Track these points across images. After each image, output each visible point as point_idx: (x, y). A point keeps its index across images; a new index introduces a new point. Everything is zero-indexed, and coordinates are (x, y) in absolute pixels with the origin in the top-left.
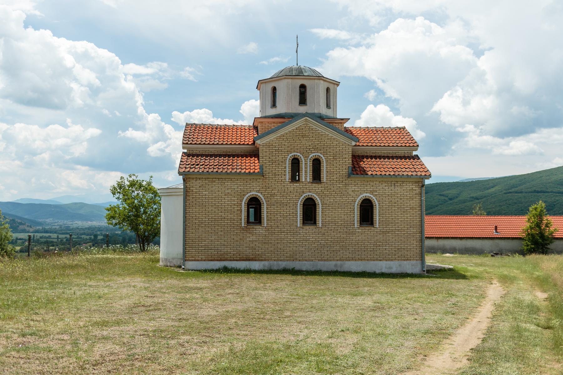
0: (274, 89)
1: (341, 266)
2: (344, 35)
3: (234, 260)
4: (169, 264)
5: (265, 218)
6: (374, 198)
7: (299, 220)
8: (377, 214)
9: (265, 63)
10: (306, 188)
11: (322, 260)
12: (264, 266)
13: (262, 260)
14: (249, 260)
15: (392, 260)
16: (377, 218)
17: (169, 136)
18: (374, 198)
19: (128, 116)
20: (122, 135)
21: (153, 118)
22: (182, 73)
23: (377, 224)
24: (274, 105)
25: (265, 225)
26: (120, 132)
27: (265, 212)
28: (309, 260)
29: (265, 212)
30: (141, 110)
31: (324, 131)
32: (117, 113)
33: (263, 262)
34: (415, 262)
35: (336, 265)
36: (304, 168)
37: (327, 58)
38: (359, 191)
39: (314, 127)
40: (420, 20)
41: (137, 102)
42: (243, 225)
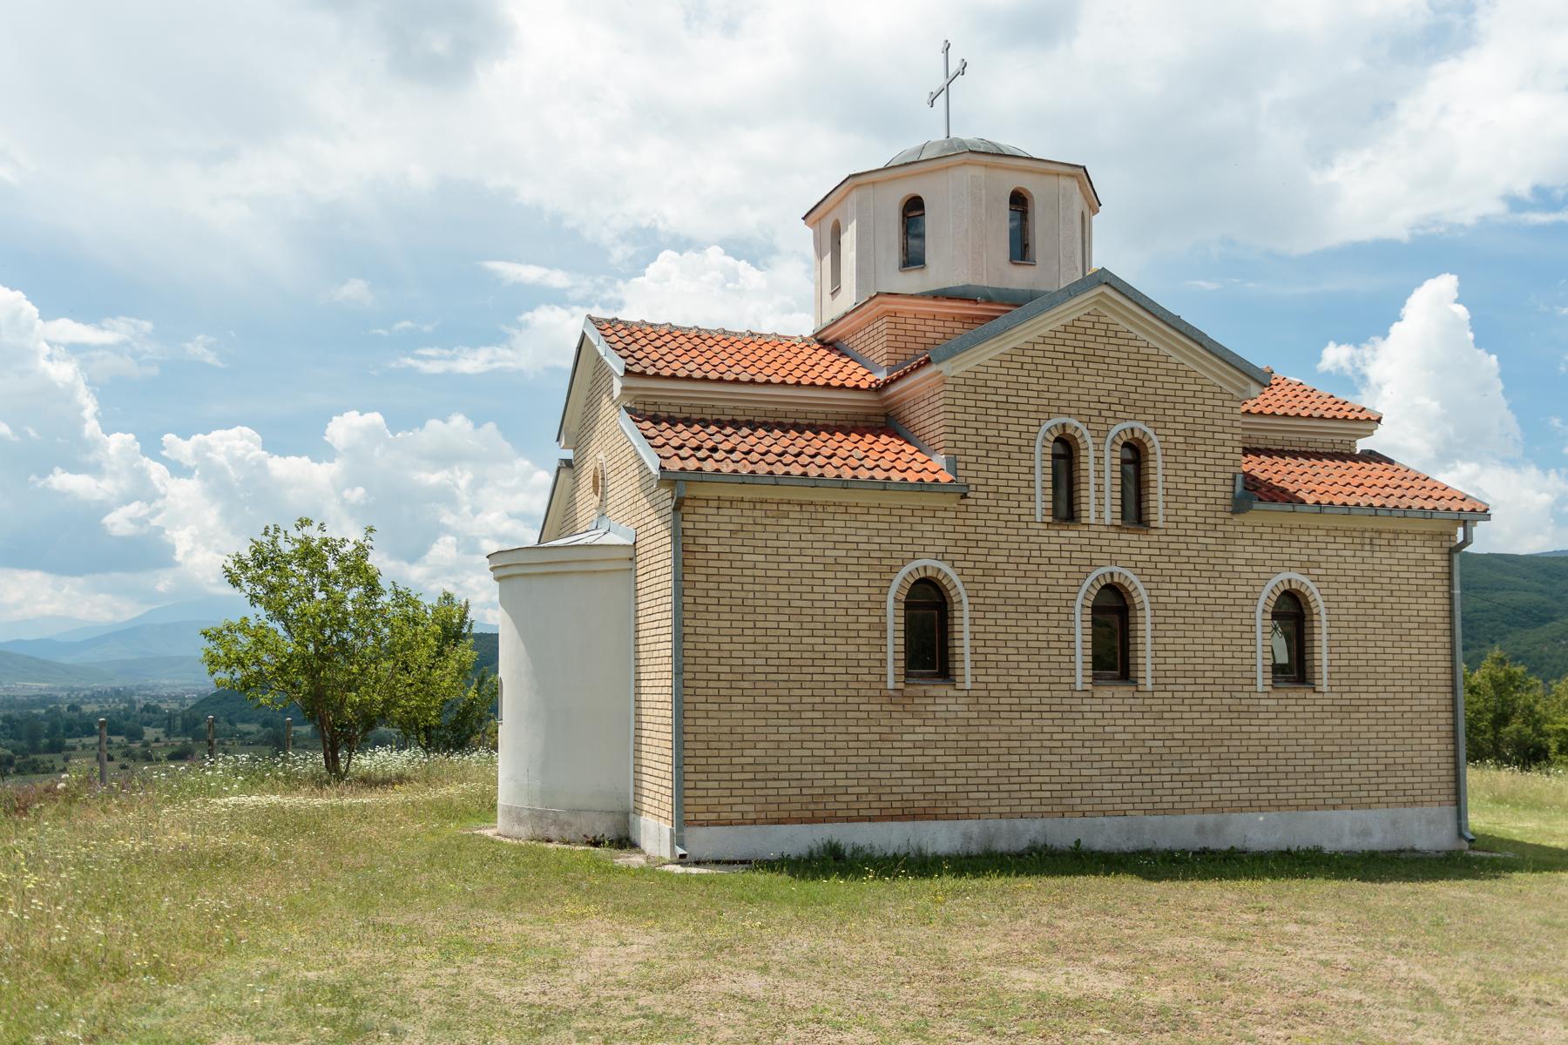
0: (914, 207)
1: (1218, 829)
2: (558, 279)
3: (861, 819)
4: (553, 832)
5: (967, 658)
6: (1313, 587)
7: (1079, 665)
8: (1325, 644)
9: (384, 332)
10: (1102, 550)
11: (1155, 812)
12: (967, 837)
13: (957, 817)
14: (914, 817)
15: (1369, 806)
16: (1325, 657)
17: (162, 490)
18: (1313, 587)
19: (59, 440)
20: (40, 484)
21: (118, 443)
22: (189, 345)
23: (1323, 683)
24: (912, 259)
25: (968, 686)
26: (33, 478)
27: (967, 636)
28: (1116, 813)
29: (967, 636)
30: (92, 428)
31: (1154, 343)
32: (32, 433)
33: (963, 825)
34: (1434, 810)
35: (1201, 829)
36: (1092, 474)
37: (522, 326)
38: (1268, 562)
39: (1124, 325)
40: (715, 254)
41: (82, 409)
42: (891, 685)
